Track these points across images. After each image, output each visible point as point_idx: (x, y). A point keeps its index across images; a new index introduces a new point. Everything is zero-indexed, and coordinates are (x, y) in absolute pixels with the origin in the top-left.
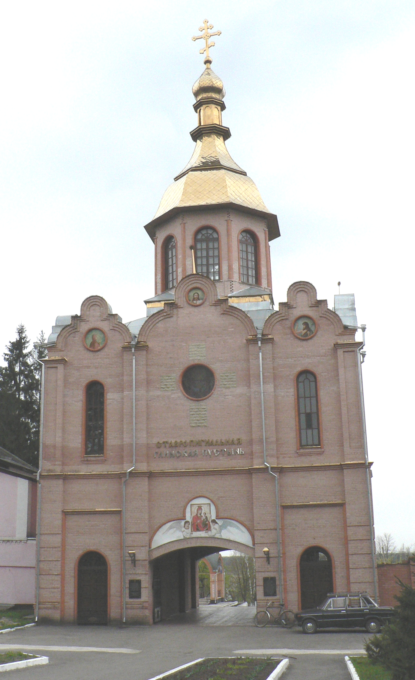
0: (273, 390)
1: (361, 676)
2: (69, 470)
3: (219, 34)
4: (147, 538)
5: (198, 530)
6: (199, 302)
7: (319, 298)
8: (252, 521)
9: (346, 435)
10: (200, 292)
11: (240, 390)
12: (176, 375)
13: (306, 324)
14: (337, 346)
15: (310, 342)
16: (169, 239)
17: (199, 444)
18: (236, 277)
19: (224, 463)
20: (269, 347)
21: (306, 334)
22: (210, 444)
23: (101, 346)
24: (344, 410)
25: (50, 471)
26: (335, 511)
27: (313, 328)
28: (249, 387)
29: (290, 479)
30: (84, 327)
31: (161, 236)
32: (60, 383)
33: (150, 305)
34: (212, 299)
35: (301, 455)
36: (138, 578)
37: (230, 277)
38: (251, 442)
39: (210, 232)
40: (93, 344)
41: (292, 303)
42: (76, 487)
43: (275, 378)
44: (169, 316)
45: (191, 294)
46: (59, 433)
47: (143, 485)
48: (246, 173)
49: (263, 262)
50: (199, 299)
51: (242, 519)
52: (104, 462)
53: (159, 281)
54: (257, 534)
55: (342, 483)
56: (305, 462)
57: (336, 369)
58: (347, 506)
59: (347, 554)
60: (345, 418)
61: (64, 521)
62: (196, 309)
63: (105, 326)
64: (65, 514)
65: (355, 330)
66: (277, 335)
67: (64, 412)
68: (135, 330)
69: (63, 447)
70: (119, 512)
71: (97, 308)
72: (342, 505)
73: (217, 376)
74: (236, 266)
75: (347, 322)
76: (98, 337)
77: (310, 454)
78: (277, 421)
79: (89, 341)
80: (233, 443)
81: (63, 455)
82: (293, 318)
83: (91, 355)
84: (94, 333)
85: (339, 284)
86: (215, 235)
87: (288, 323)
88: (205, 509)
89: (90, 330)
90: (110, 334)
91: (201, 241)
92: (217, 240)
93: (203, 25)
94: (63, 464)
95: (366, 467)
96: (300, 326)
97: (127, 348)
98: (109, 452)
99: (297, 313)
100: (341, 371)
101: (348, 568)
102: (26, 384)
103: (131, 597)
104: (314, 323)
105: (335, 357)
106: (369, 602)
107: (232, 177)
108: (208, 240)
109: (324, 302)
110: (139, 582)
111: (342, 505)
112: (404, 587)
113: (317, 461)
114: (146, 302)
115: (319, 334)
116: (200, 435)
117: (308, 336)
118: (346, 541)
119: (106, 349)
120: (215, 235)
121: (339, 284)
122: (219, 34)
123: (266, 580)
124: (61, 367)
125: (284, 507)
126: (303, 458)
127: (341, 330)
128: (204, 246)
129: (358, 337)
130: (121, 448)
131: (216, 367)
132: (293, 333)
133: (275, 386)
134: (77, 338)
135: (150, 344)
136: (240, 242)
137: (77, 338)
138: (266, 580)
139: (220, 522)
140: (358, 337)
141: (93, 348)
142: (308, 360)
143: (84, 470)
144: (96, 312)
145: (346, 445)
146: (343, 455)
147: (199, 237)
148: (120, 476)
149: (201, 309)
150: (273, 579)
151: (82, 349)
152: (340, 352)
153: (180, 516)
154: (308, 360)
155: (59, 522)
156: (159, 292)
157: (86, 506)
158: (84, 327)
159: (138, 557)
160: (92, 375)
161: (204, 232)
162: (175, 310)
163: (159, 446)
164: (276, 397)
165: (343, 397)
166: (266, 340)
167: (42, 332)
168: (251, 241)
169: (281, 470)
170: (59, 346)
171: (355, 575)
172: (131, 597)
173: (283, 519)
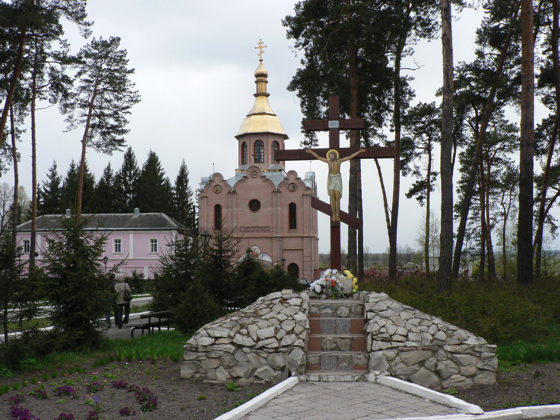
3: (266, 47)
6: (255, 176)
7: (298, 177)
9: (305, 226)
11: (269, 209)
12: (247, 203)
13: (293, 186)
14: (303, 195)
15: (295, 193)
17: (255, 227)
18: (270, 161)
19: (263, 234)
21: (293, 190)
24: (305, 217)
26: (301, 252)
27: (295, 187)
28: (272, 207)
29: (285, 240)
30: (213, 184)
31: (242, 141)
32: (205, 205)
33: (237, 171)
34: (260, 176)
35: (289, 232)
37: (268, 161)
38: (272, 227)
39: (260, 142)
40: (217, 191)
41: (288, 178)
43: (281, 205)
44: (244, 181)
45: (253, 173)
46: (205, 223)
48: (286, 135)
53: (240, 160)
55: (303, 241)
59: (303, 266)
60: (305, 220)
63: (221, 184)
68: (232, 184)
72: (303, 250)
73: (261, 204)
74: (270, 157)
76: (219, 188)
77: (293, 232)
79: (216, 189)
82: (289, 183)
86: (262, 144)
87: (287, 185)
88: (256, 250)
90: (223, 187)
91: (257, 146)
92: (263, 146)
93: (259, 42)
96: (291, 186)
97: (229, 193)
99: (290, 182)
100: (304, 203)
104: (296, 186)
105: (303, 199)
106: (307, 281)
108: (259, 146)
109: (300, 178)
111: (303, 250)
112: (213, 338)
114: (236, 170)
116: (255, 224)
117: (293, 190)
119: (221, 193)
120: (262, 144)
122: (266, 47)
124: (205, 199)
125: (284, 250)
126: (290, 234)
128: (258, 148)
131: (261, 201)
134: (211, 188)
136: (272, 146)
137: (211, 188)
139: (261, 254)
141: (217, 192)
145: (305, 229)
146: (303, 232)
147: (256, 144)
151: (213, 192)
152: (304, 197)
156: (240, 164)
158: (213, 184)
161: (258, 142)
163: (241, 228)
166: (278, 191)
168: (276, 145)
169: (282, 237)
170: (205, 191)
171: (306, 273)
173: (283, 254)
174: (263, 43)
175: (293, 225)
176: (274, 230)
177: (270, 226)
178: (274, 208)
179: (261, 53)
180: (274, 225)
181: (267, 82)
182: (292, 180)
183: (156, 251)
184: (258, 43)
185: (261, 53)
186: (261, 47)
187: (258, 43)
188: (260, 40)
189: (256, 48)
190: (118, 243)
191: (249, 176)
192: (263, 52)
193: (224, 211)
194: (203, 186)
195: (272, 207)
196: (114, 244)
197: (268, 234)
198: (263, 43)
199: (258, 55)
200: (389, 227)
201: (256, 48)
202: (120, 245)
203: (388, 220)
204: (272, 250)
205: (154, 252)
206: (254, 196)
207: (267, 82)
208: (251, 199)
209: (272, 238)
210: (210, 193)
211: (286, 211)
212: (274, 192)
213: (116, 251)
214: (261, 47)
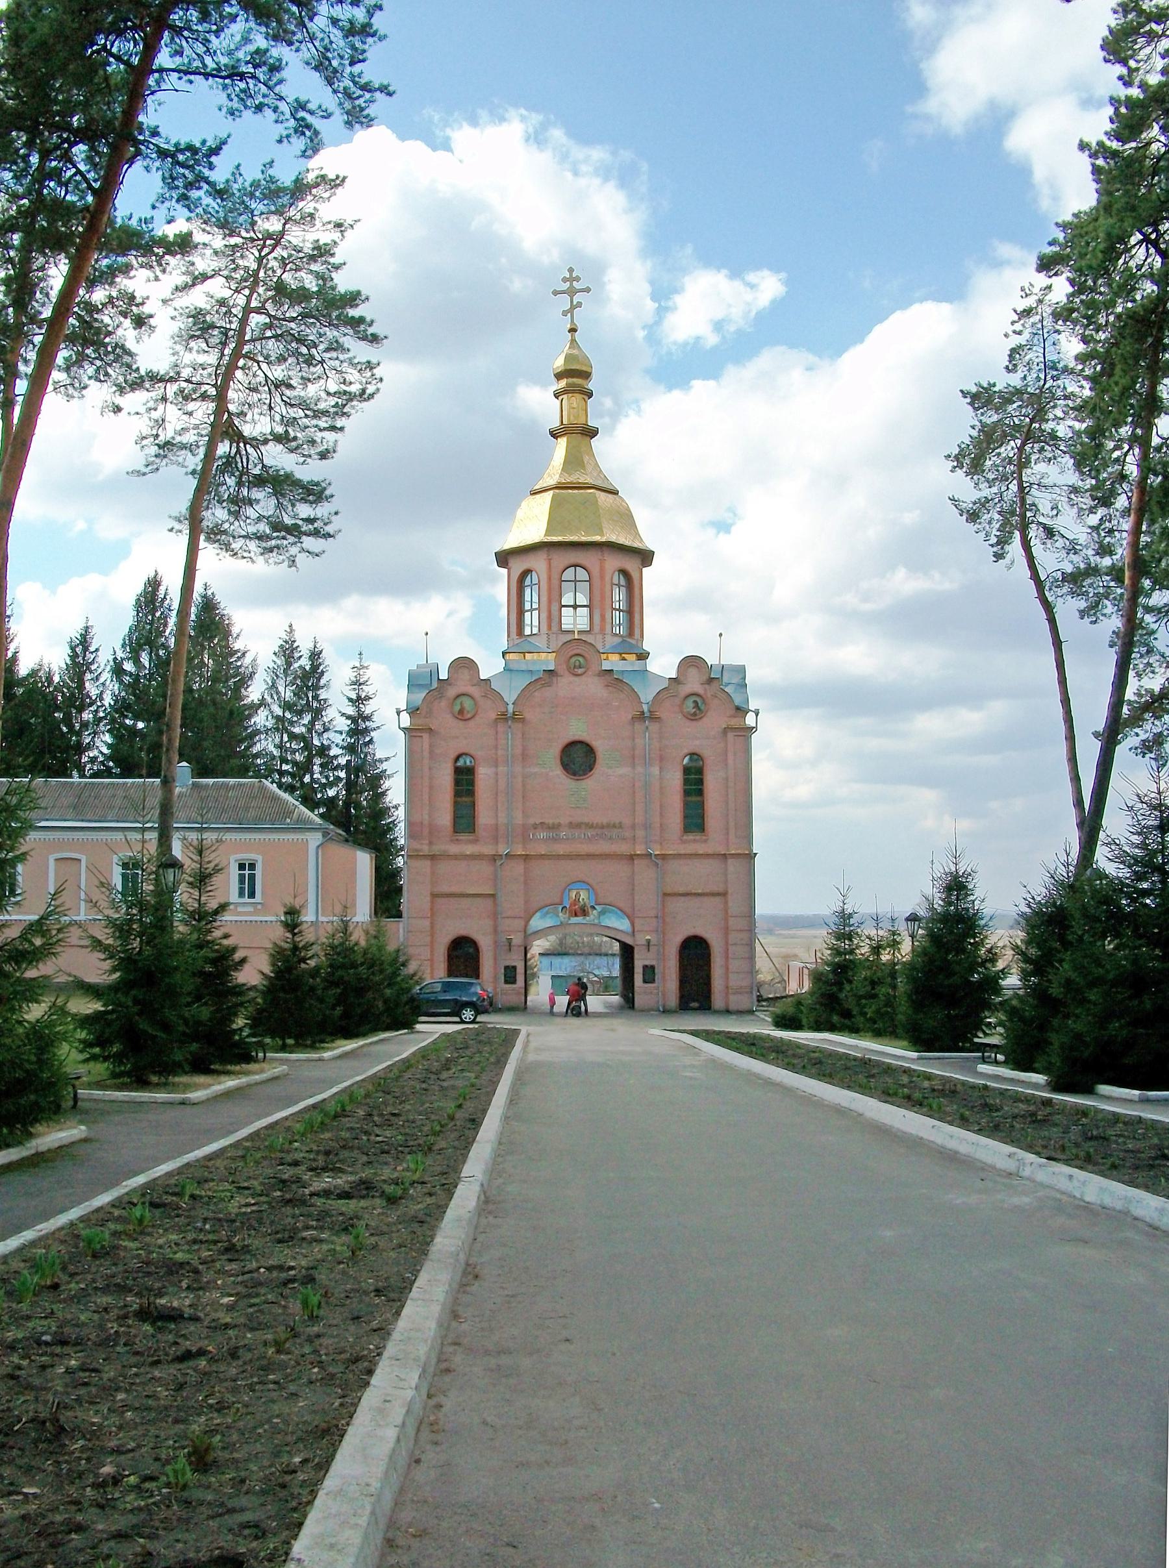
0: (657, 772)
1: (5, 1259)
2: (437, 848)
4: (522, 923)
5: (576, 915)
6: (580, 671)
8: (633, 908)
10: (581, 659)
11: (624, 770)
12: (555, 750)
13: (695, 702)
14: (725, 731)
16: (526, 573)
19: (604, 847)
20: (654, 727)
21: (695, 714)
22: (590, 826)
23: (469, 716)
25: (417, 850)
26: (717, 900)
27: (702, 708)
28: (633, 766)
29: (673, 865)
30: (451, 692)
32: (426, 754)
35: (683, 842)
36: (514, 964)
38: (633, 827)
40: (461, 712)
41: (682, 678)
42: (444, 867)
43: (661, 759)
45: (573, 660)
47: (518, 868)
49: (637, 609)
50: (580, 667)
51: (621, 905)
52: (476, 841)
54: (637, 921)
56: (690, 849)
57: (725, 752)
58: (729, 897)
59: (727, 943)
61: (432, 902)
62: (576, 679)
63: (474, 691)
64: (434, 896)
65: (747, 711)
66: (663, 713)
67: (431, 787)
69: (430, 825)
70: (493, 896)
71: (466, 671)
75: (738, 701)
76: (468, 703)
78: (661, 806)
79: (457, 708)
80: (614, 826)
81: (430, 833)
82: (683, 693)
83: (461, 724)
84: (464, 699)
85: (721, 635)
87: (677, 701)
89: (458, 696)
94: (431, 843)
95: (751, 856)
96: (690, 704)
97: (503, 717)
98: (480, 830)
101: (727, 958)
102: (309, 717)
103: (506, 982)
107: (310, 45)
110: (514, 968)
113: (701, 849)
115: (709, 714)
118: (726, 930)
119: (477, 718)
121: (721, 635)
122: (588, 290)
123: (645, 967)
125: (665, 895)
127: (733, 712)
129: (750, 720)
130: (496, 828)
131: (597, 744)
132: (682, 712)
133: (661, 769)
135: (527, 715)
138: (645, 967)
140: (750, 720)
142: (697, 742)
143: (454, 849)
144: (465, 675)
145: (732, 832)
148: (494, 858)
149: (583, 678)
150: (653, 967)
152: (730, 735)
153: (557, 900)
154: (697, 742)
155: (427, 906)
157: (455, 889)
158: (451, 692)
159: (514, 942)
160: (461, 746)
162: (555, 679)
163: (535, 826)
164: (661, 778)
165: (731, 784)
166: (653, 718)
167: (291, 626)
169: (664, 857)
172: (506, 982)
174: (578, 279)
175: (695, 820)
176: (640, 833)
177: (627, 822)
178: (640, 769)
179: (573, 307)
180: (639, 819)
181: (590, 395)
182: (694, 684)
183: (252, 895)
184: (565, 280)
185: (573, 307)
186: (572, 292)
187: (565, 280)
188: (571, 270)
189: (556, 293)
190: (247, 872)
191: (562, 669)
192: (579, 305)
193: (484, 775)
194: (420, 696)
195: (633, 766)
196: (234, 872)
197: (624, 848)
198: (578, 279)
199: (565, 313)
200: (1080, 825)
201: (556, 293)
202: (252, 878)
203: (1079, 803)
204: (633, 894)
205: (246, 900)
206: (577, 730)
207: (590, 395)
208: (566, 741)
209: (632, 858)
210: (443, 720)
211: (675, 780)
212: (641, 717)
213: (241, 894)
214: (572, 292)
